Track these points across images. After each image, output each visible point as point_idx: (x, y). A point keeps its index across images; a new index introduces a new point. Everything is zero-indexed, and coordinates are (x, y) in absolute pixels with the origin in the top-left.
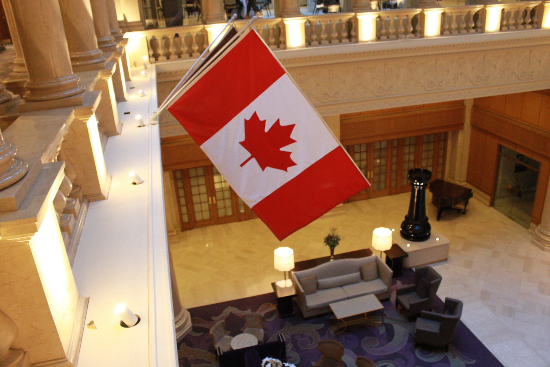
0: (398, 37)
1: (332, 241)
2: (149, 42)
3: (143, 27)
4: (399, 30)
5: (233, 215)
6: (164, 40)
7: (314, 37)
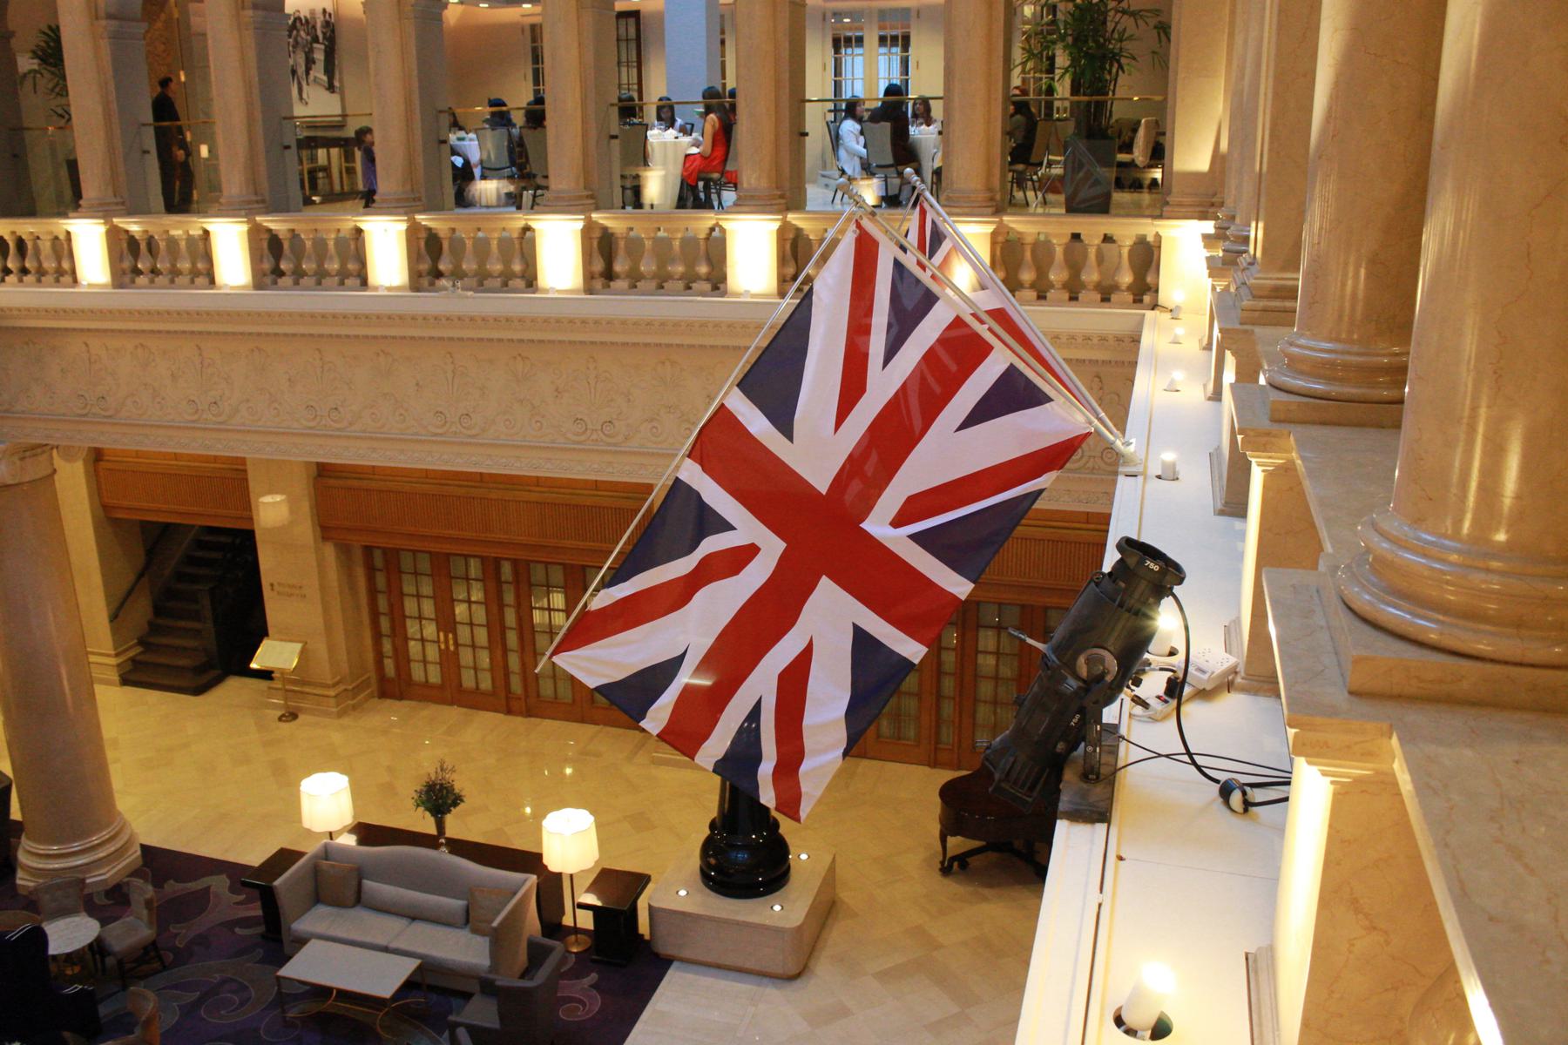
0: (505, 286)
1: (439, 799)
5: (494, 693)
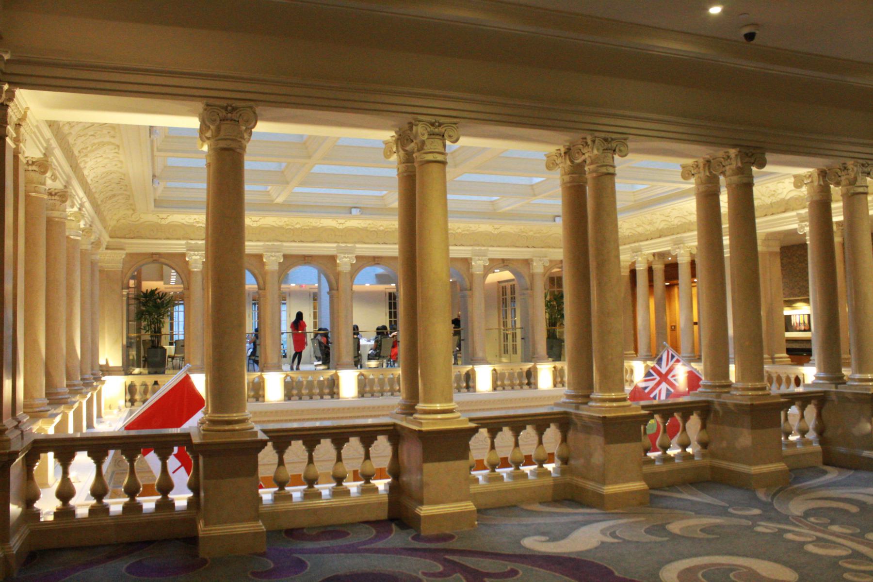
2: (127, 387)
3: (123, 373)
4: (385, 388)
6: (143, 387)
7: (295, 392)
